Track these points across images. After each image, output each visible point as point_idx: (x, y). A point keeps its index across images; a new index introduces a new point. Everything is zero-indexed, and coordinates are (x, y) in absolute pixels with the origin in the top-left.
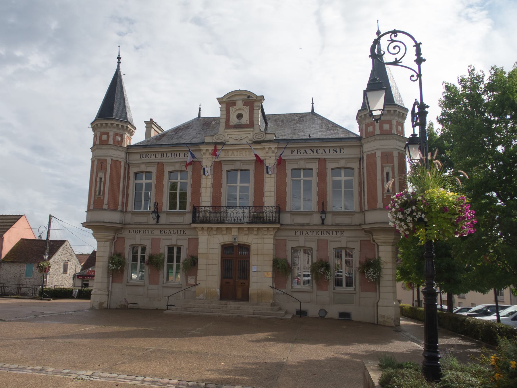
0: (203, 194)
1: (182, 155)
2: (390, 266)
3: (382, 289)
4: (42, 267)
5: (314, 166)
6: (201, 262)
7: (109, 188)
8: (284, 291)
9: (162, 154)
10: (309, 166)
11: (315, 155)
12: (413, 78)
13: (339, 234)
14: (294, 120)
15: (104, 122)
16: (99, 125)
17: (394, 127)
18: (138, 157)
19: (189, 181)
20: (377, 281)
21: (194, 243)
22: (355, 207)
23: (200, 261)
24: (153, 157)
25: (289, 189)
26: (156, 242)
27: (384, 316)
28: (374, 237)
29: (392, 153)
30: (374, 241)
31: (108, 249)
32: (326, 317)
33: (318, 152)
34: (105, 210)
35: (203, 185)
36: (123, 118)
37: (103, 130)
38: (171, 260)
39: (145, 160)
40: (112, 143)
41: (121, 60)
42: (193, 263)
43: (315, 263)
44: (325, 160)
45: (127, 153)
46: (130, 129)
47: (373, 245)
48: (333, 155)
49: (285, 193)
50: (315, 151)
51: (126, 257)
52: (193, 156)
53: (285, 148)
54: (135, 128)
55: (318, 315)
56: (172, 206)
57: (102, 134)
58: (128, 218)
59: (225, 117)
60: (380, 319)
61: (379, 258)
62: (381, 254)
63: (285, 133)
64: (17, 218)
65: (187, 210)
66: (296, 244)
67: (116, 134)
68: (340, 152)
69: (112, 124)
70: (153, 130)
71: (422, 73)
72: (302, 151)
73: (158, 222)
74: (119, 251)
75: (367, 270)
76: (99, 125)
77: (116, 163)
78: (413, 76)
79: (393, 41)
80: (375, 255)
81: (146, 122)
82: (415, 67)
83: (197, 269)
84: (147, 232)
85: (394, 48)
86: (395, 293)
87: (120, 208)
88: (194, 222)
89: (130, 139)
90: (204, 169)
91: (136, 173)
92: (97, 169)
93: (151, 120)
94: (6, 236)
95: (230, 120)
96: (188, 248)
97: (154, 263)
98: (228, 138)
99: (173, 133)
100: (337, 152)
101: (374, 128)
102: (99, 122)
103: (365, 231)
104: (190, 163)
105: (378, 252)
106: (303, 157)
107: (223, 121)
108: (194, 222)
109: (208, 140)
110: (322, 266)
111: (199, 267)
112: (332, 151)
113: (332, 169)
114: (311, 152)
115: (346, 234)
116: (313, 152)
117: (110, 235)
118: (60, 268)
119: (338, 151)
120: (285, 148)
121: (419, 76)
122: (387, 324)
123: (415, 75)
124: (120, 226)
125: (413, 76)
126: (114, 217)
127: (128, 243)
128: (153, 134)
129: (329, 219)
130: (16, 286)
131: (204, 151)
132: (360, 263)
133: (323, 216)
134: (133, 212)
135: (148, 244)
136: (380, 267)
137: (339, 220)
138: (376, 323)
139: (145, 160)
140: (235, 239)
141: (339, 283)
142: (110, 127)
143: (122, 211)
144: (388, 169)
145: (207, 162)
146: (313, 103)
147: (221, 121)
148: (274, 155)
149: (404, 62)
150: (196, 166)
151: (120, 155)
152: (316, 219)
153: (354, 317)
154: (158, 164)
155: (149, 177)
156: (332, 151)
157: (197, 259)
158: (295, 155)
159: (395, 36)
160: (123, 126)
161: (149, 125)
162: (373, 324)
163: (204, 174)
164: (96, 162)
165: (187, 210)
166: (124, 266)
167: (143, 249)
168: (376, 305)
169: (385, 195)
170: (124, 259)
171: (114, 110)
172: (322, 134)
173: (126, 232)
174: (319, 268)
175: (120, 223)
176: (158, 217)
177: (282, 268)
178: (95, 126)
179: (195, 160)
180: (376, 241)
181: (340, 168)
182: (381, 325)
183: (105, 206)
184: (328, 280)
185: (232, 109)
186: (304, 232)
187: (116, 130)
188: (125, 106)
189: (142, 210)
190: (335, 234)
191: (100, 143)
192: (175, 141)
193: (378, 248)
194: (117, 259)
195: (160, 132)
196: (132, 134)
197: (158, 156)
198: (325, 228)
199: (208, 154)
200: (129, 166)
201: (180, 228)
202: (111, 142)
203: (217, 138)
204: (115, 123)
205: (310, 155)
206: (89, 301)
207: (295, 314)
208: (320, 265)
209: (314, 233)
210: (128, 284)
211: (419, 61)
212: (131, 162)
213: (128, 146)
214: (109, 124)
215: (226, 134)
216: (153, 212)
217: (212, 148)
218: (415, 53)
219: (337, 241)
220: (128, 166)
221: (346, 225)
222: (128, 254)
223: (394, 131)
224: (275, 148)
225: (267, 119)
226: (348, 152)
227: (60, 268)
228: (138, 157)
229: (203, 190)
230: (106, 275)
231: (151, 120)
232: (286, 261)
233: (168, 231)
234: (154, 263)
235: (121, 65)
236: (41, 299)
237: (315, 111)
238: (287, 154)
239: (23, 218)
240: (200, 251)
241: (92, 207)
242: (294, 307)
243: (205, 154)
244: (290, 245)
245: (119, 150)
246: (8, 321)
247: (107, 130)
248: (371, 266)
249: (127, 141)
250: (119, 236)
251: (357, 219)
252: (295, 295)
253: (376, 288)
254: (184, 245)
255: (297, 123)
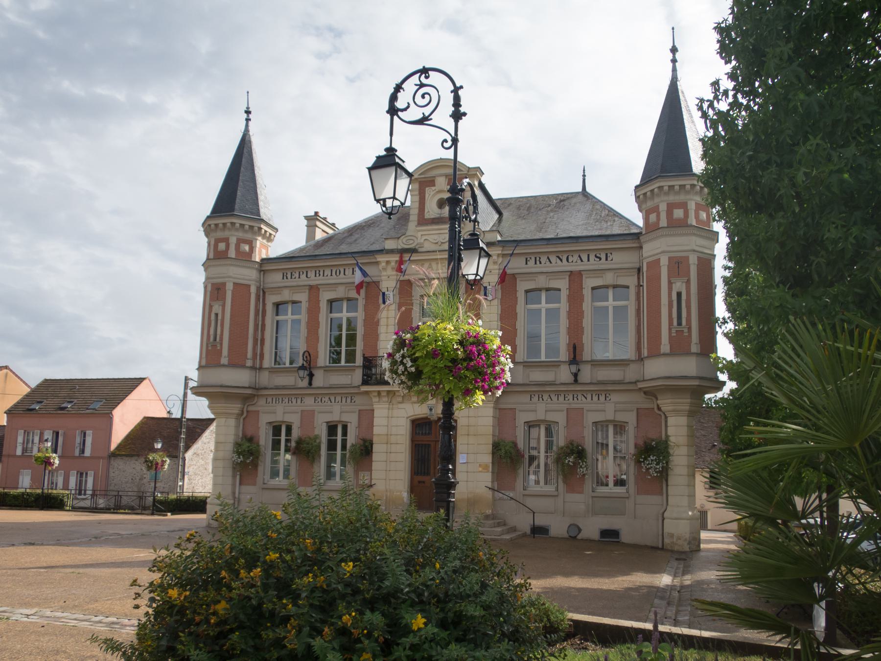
0: (382, 337)
1: (349, 272)
2: (684, 450)
3: (671, 490)
4: (151, 462)
5: (563, 284)
6: (378, 449)
7: (230, 331)
8: (511, 495)
9: (317, 270)
10: (554, 284)
11: (565, 266)
12: (445, 145)
13: (602, 398)
14: (550, 205)
15: (220, 221)
16: (213, 226)
17: (692, 214)
18: (278, 277)
19: (359, 315)
20: (664, 474)
21: (367, 417)
22: (629, 353)
23: (375, 448)
24: (303, 277)
25: (587, 322)
26: (307, 417)
27: (672, 536)
28: (659, 402)
29: (687, 258)
30: (659, 409)
31: (232, 431)
32: (579, 537)
33: (570, 260)
34: (224, 366)
35: (383, 322)
36: (252, 213)
37: (220, 234)
38: (332, 446)
39: (289, 282)
40: (234, 256)
41: (251, 116)
42: (365, 451)
43: (562, 448)
44: (580, 273)
45: (261, 271)
46: (266, 231)
47: (658, 417)
48: (593, 264)
49: (582, 329)
50: (564, 259)
51: (262, 442)
52: (365, 274)
53: (511, 255)
54: (276, 230)
55: (566, 535)
56: (335, 358)
57: (218, 241)
58: (264, 379)
59: (417, 205)
60: (667, 541)
61: (667, 436)
62: (671, 431)
63: (525, 230)
64: (137, 382)
65: (357, 364)
66: (531, 417)
67: (240, 241)
68: (607, 259)
69: (233, 224)
70: (317, 230)
71: (459, 137)
72: (544, 259)
73: (310, 384)
74: (249, 433)
75: (645, 459)
76: (213, 226)
77: (241, 289)
78: (445, 141)
79: (422, 85)
80: (661, 432)
81: (307, 218)
82: (450, 124)
83: (371, 461)
84: (294, 401)
85: (423, 97)
86: (692, 496)
87: (249, 363)
88: (365, 382)
89: (267, 248)
90: (384, 294)
91: (331, 302)
92: (211, 299)
93: (316, 213)
94: (117, 413)
95: (426, 211)
96: (359, 426)
97: (305, 451)
98: (422, 241)
99: (346, 235)
100: (600, 259)
101: (658, 216)
102: (212, 222)
103: (645, 393)
104: (359, 287)
105: (666, 426)
106: (545, 270)
107: (414, 212)
108: (365, 382)
109: (390, 245)
110: (572, 452)
111: (375, 456)
112: (592, 257)
113: (593, 289)
114: (558, 260)
115: (614, 397)
116: (561, 260)
117: (235, 407)
118: (207, 463)
119: (603, 257)
120: (511, 255)
121: (455, 141)
122: (676, 548)
123: (449, 139)
124: (249, 391)
125: (445, 141)
126: (240, 378)
127: (265, 419)
128: (319, 235)
129: (586, 373)
130: (135, 494)
131: (384, 264)
132: (636, 445)
133: (574, 368)
134: (272, 368)
135: (295, 420)
136: (668, 453)
137: (604, 374)
138: (660, 546)
139: (289, 282)
140: (431, 410)
141: (602, 482)
142: (229, 229)
143: (253, 368)
144: (679, 286)
145: (389, 283)
146: (584, 176)
147: (412, 212)
148: (496, 267)
149: (435, 120)
150: (371, 290)
151: (248, 275)
152: (565, 374)
153: (625, 538)
154: (311, 287)
155: (353, 307)
156: (592, 257)
157: (372, 445)
158: (532, 267)
159: (427, 77)
160: (251, 227)
161: (312, 223)
162: (657, 548)
163: (384, 302)
164: (209, 288)
165: (357, 364)
166: (257, 458)
167: (289, 429)
168: (660, 516)
169: (674, 331)
170: (258, 445)
171: (238, 201)
172: (586, 229)
173: (262, 401)
174: (569, 455)
175: (249, 388)
176: (311, 376)
177: (507, 457)
178: (208, 227)
179: (367, 279)
180: (662, 409)
181: (607, 287)
182: (667, 550)
183: (224, 361)
184: (584, 475)
185: (429, 192)
186: (546, 397)
187: (241, 234)
188: (256, 193)
189: (543, 358)
190: (595, 398)
191: (217, 256)
192: (344, 248)
193: (666, 422)
194: (246, 445)
195: (331, 232)
196: (269, 239)
197: (311, 274)
198: (578, 388)
199: (389, 268)
200: (264, 293)
201: (346, 393)
202: (232, 253)
203: (404, 241)
204: (238, 221)
205: (557, 265)
206: (203, 516)
207: (528, 531)
208: (569, 451)
209: (561, 398)
210: (265, 486)
211: (457, 115)
212: (267, 286)
213: (263, 260)
214: (229, 225)
215: (420, 234)
216: (302, 368)
217: (396, 258)
218: (452, 102)
219: (598, 410)
220: (262, 293)
221: (614, 383)
222: (265, 438)
223: (692, 221)
224: (498, 255)
225: (498, 204)
226: (620, 259)
227: (207, 463)
228: (278, 277)
229: (382, 329)
230: (230, 472)
231: (316, 213)
232: (515, 444)
233: (327, 399)
234: (305, 451)
235: (250, 123)
236: (153, 514)
237: (589, 189)
238: (517, 265)
239: (145, 382)
240: (376, 430)
241: (204, 363)
242: (524, 523)
243: (385, 269)
244: (523, 418)
245: (651, 256)
246: (38, 545)
247: (682, 198)
248: (653, 452)
249: (260, 251)
250: (251, 408)
251: (631, 373)
252: (529, 502)
253: (662, 489)
254: (352, 420)
255: (552, 211)
